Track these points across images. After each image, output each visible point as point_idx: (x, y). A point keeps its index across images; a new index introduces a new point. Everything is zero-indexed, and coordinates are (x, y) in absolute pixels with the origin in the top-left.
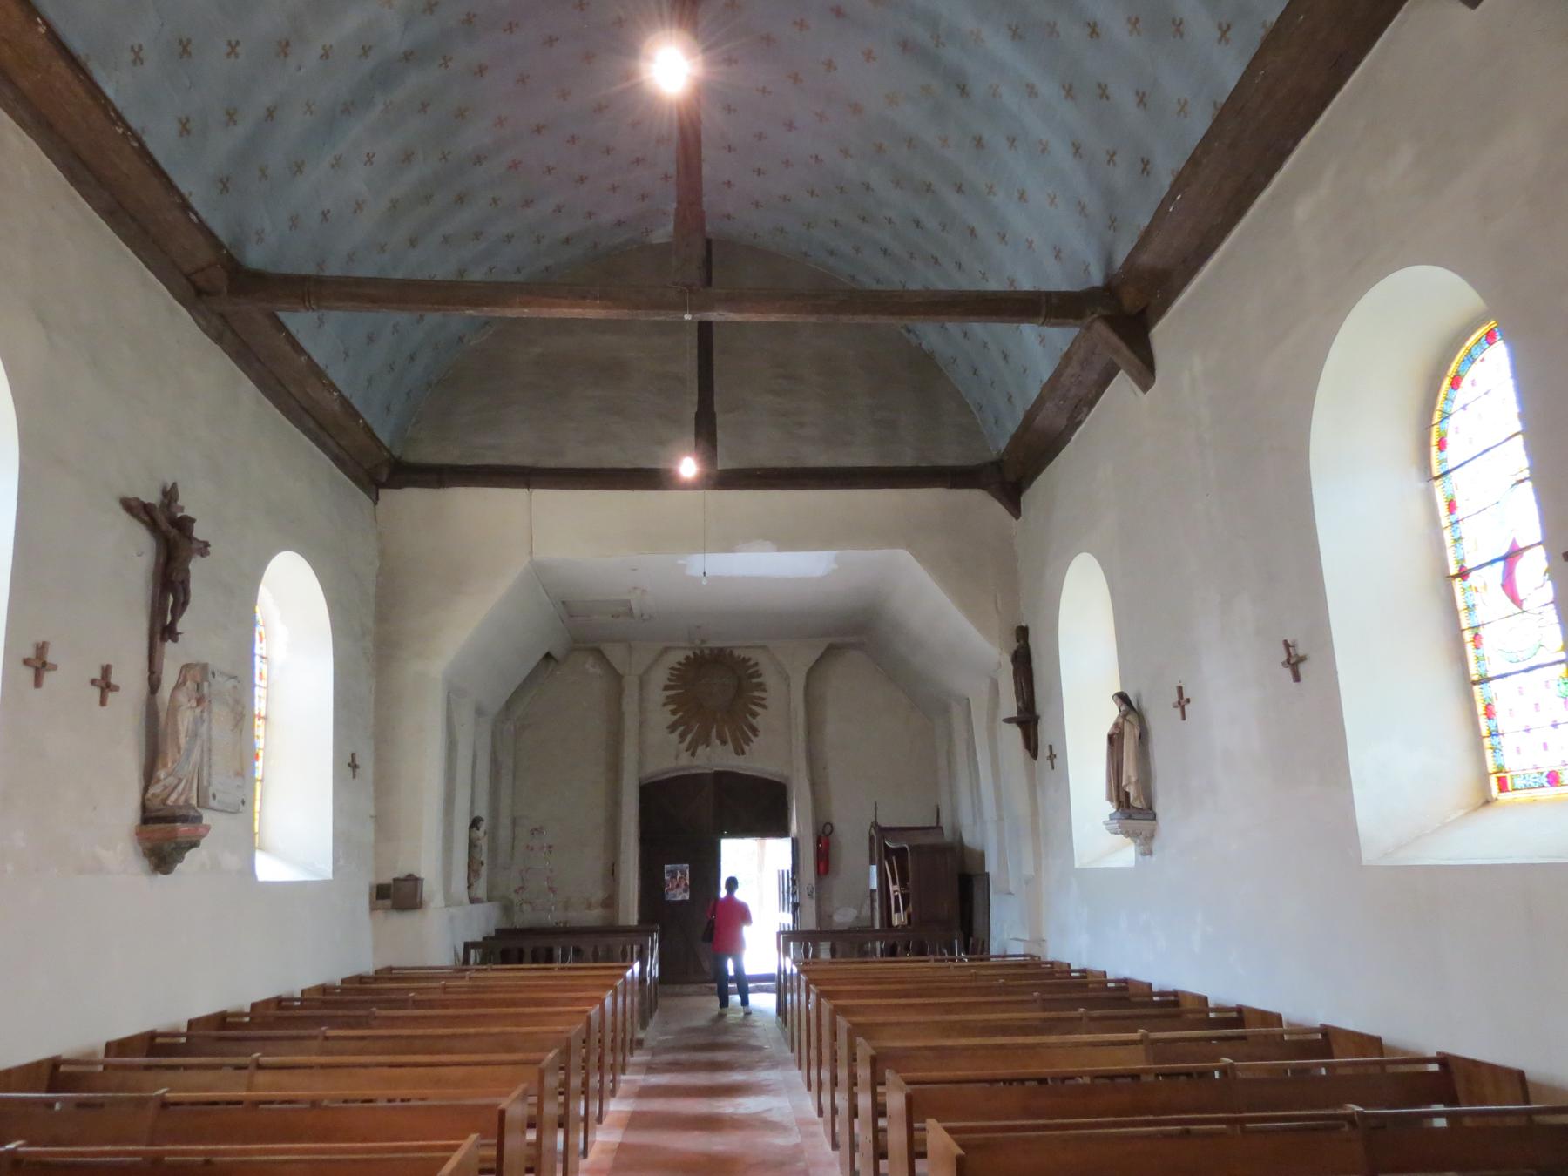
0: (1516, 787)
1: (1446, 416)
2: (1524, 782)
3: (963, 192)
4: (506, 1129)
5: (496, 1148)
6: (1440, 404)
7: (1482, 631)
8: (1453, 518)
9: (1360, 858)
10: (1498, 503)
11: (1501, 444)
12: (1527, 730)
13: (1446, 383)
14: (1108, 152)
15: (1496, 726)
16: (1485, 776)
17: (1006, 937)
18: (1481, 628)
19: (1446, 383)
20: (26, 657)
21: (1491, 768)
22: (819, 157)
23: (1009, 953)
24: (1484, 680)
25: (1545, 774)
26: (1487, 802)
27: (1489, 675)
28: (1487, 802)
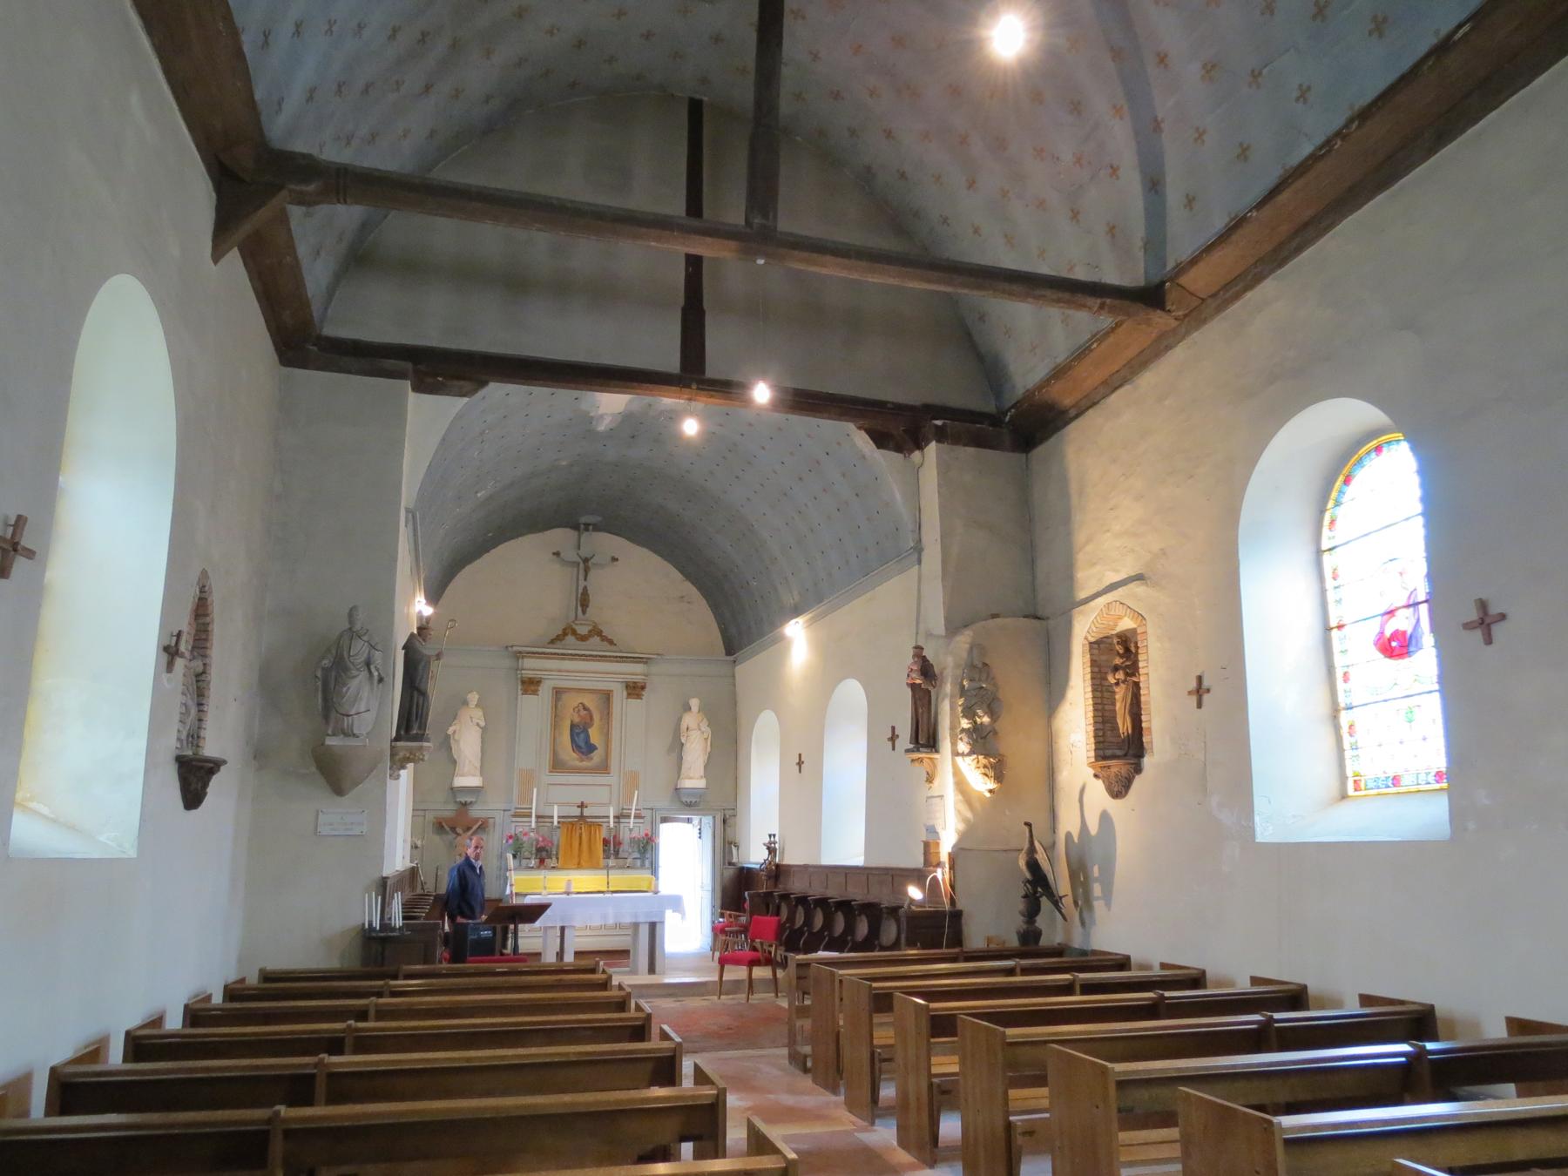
0: (1368, 787)
1: (1338, 504)
2: (1375, 784)
3: (1158, 54)
4: (1505, 1159)
5: (1010, 1098)
6: (1334, 494)
7: (1350, 670)
8: (1336, 583)
9: (1251, 830)
10: (1362, 580)
11: (1358, 538)
12: (1424, 739)
13: (1341, 478)
14: (1108, 224)
15: (1356, 742)
16: (1343, 778)
17: (508, 892)
18: (1350, 668)
19: (1341, 478)
20: (166, 645)
21: (1349, 773)
22: (421, 762)
23: (573, 890)
24: (1350, 708)
25: (1433, 774)
26: (1344, 796)
27: (1354, 704)
28: (1344, 796)
